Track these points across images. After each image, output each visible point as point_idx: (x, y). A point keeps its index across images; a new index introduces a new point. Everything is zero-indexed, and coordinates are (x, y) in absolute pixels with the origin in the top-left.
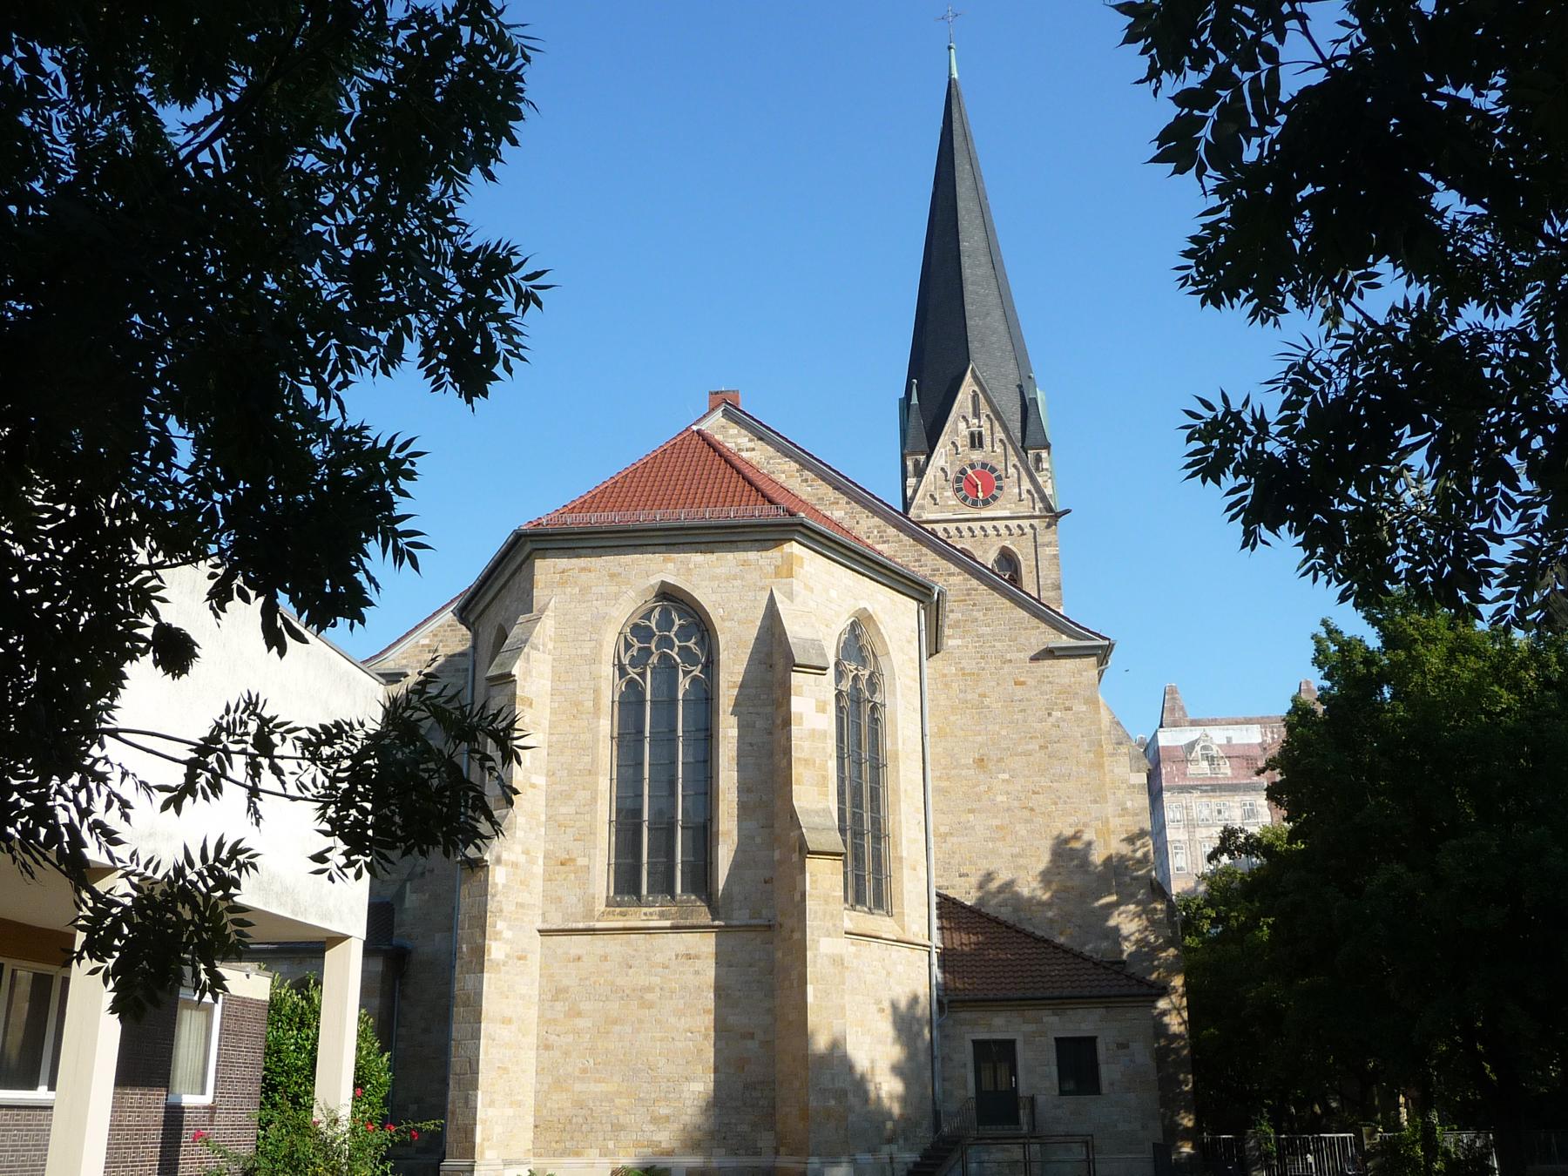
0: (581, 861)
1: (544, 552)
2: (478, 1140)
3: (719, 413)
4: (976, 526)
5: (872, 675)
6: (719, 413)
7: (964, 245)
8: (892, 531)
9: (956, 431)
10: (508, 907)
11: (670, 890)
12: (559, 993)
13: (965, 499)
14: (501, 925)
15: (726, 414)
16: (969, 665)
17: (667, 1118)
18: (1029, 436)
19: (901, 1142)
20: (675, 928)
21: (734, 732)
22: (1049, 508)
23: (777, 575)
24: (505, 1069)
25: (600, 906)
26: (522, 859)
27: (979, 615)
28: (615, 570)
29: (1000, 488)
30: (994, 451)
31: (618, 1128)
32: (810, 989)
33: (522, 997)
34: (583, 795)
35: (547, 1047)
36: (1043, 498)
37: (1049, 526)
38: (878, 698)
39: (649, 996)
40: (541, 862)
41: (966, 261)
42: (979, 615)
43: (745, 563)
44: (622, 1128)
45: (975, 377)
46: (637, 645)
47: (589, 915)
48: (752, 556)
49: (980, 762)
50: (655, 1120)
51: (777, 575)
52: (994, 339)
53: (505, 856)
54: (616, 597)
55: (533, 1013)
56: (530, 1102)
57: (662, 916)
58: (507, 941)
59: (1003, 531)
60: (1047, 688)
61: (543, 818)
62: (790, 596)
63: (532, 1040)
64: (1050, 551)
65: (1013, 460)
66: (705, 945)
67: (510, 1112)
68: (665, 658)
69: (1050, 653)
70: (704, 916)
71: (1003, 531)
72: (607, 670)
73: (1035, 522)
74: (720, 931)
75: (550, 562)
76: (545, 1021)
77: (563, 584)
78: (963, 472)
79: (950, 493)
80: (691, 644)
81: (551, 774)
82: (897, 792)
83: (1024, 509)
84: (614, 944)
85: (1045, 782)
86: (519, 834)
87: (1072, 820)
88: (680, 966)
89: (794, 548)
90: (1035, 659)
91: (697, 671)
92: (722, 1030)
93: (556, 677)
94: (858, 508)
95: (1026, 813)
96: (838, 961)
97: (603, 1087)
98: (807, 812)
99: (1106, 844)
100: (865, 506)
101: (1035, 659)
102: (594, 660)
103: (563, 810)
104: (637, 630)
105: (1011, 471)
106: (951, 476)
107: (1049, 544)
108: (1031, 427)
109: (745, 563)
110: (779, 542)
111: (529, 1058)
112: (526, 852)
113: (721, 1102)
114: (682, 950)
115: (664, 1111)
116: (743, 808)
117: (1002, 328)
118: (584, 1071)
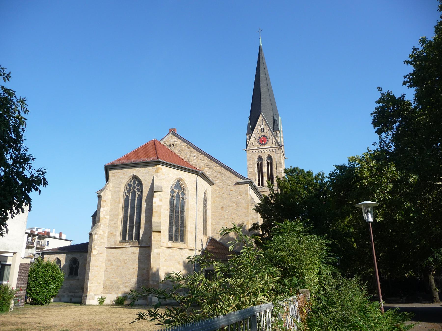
0: (115, 233)
1: (111, 169)
2: (88, 290)
3: (171, 133)
4: (262, 150)
5: (183, 192)
6: (171, 133)
7: (261, 85)
8: (206, 158)
9: (258, 128)
10: (98, 243)
11: (132, 239)
12: (109, 260)
13: (260, 144)
14: (96, 247)
15: (172, 134)
16: (220, 187)
17: (128, 286)
18: (275, 128)
19: (184, 292)
20: (131, 247)
21: (145, 206)
22: (279, 145)
23: (155, 172)
24: (96, 276)
25: (118, 242)
26: (102, 233)
27: (223, 176)
28: (124, 172)
29: (268, 141)
30: (267, 133)
31: (118, 288)
32: (152, 260)
33: (101, 261)
34: (116, 220)
35: (106, 272)
36: (278, 143)
37: (279, 149)
38: (184, 197)
39: (126, 261)
40: (107, 234)
41: (261, 88)
42: (223, 176)
43: (149, 170)
44: (119, 288)
45: (262, 115)
46: (128, 188)
47: (115, 244)
48: (151, 168)
49: (222, 208)
50: (125, 287)
51: (155, 172)
52: (267, 106)
53: (97, 233)
54: (124, 178)
55: (104, 265)
56: (102, 283)
57: (129, 244)
58: (97, 250)
59: (268, 151)
60: (237, 191)
61: (108, 225)
62: (158, 176)
63: (103, 270)
64: (279, 155)
65: (271, 134)
66: (137, 250)
67: (97, 285)
68: (134, 190)
69: (238, 183)
70: (137, 245)
71: (268, 151)
72: (122, 194)
73: (276, 148)
74: (140, 247)
75: (112, 171)
76: (106, 266)
77: (114, 176)
78: (259, 138)
79: (256, 143)
80: (139, 187)
81: (110, 215)
82: (188, 217)
83: (273, 146)
84: (119, 251)
85: (236, 212)
86: (101, 228)
87: (241, 220)
88: (133, 254)
89: (159, 166)
90: (235, 185)
91: (140, 193)
92: (139, 268)
93: (112, 195)
94: (199, 153)
95: (231, 219)
96: (159, 254)
97: (116, 280)
98: (155, 223)
99: (248, 226)
100: (200, 153)
101: (235, 185)
102: (119, 192)
103: (112, 223)
104: (129, 185)
105: (270, 137)
106: (257, 139)
107: (279, 153)
108: (275, 126)
109: (149, 170)
110: (156, 165)
111: (102, 274)
112: (103, 232)
113: (138, 282)
114: (132, 252)
115: (127, 285)
116: (146, 221)
117: (270, 103)
118: (113, 276)
